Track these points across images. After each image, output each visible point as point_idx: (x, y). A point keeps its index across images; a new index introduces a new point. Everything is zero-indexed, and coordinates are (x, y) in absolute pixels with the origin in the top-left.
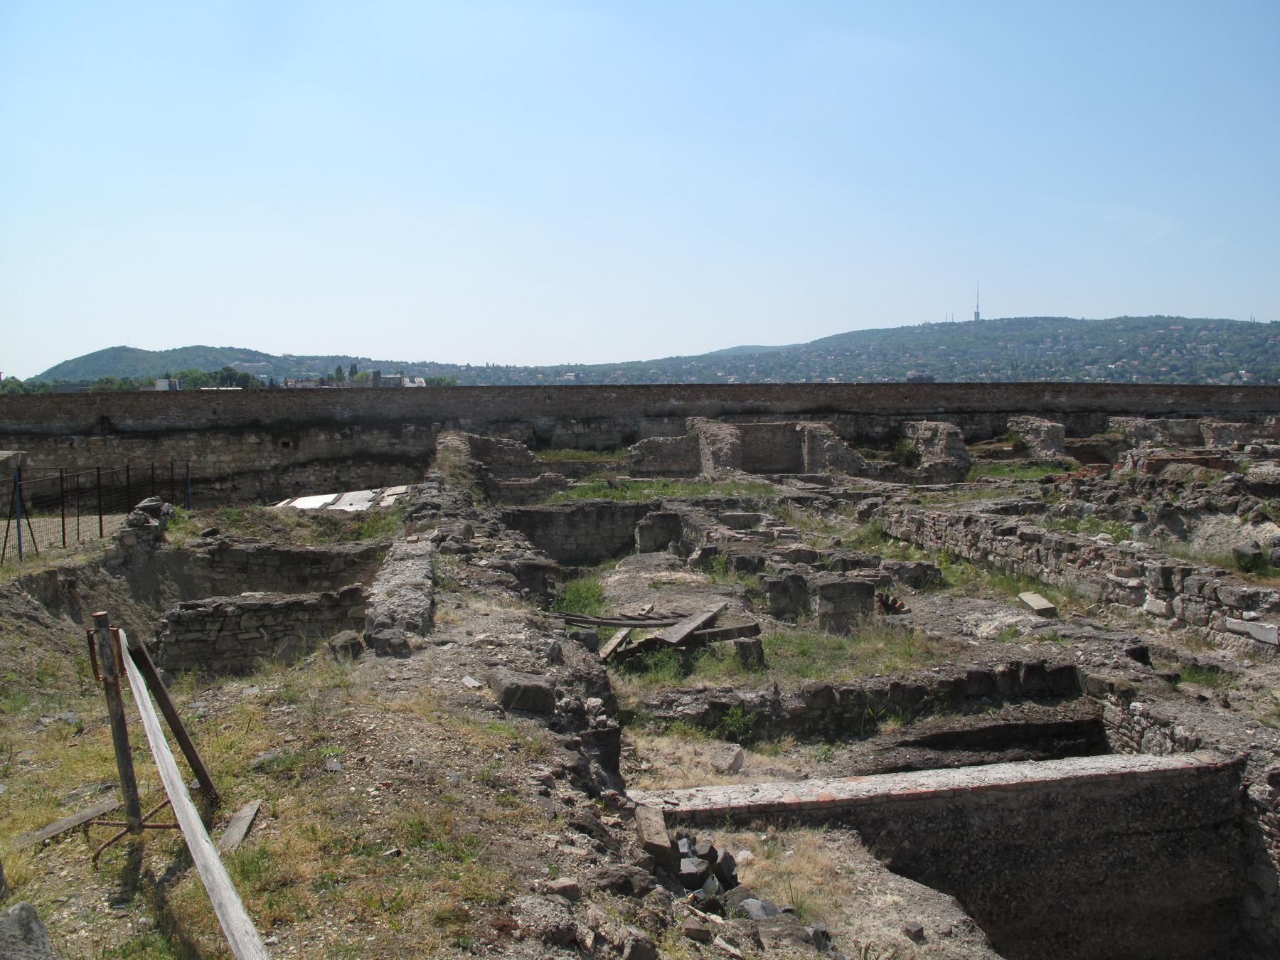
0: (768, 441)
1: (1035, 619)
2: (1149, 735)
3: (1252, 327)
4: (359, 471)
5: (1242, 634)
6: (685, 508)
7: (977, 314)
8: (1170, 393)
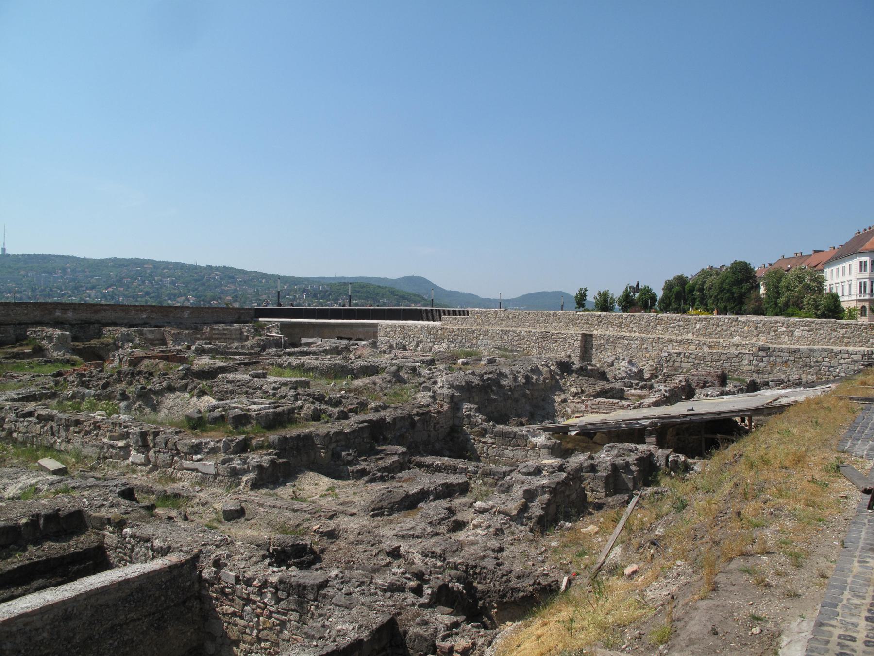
2: (137, 549)
3: (195, 268)
5: (193, 470)
8: (144, 311)
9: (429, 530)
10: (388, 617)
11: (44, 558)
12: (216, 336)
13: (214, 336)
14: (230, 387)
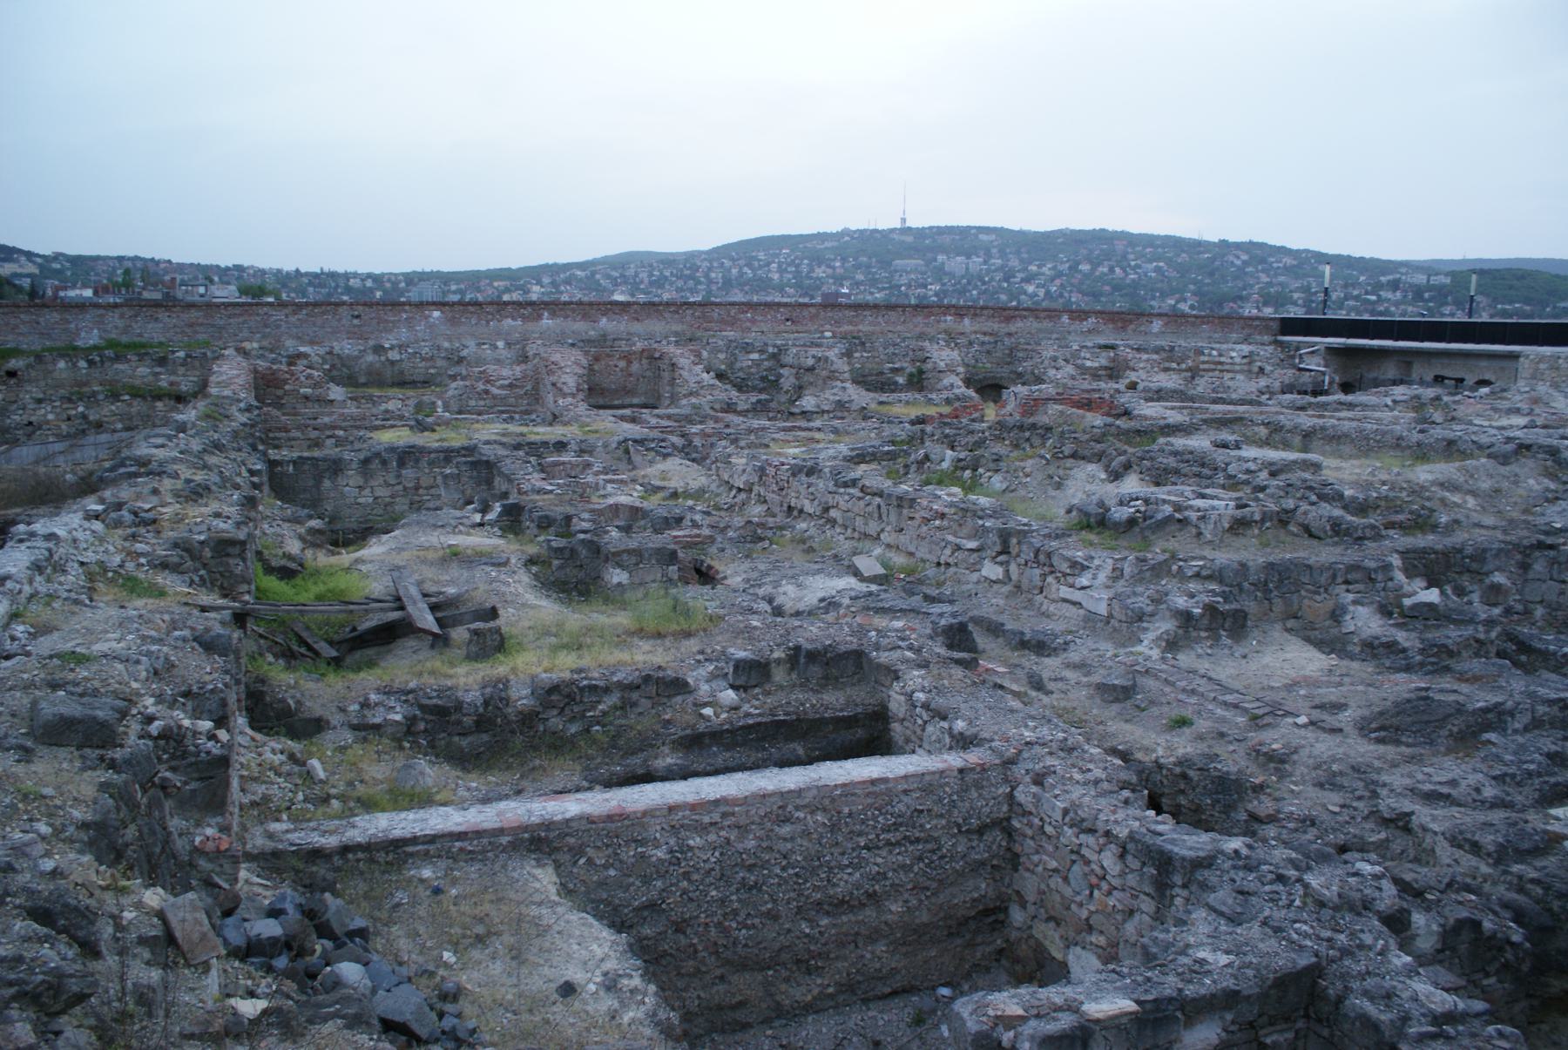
0: (622, 370)
1: (863, 587)
2: (930, 729)
3: (1196, 246)
4: (113, 408)
5: (1074, 603)
6: (502, 452)
7: (904, 220)
9: (1489, 792)
10: (1304, 961)
11: (794, 717)
12: (1206, 366)
13: (1202, 366)
14: (1171, 462)
